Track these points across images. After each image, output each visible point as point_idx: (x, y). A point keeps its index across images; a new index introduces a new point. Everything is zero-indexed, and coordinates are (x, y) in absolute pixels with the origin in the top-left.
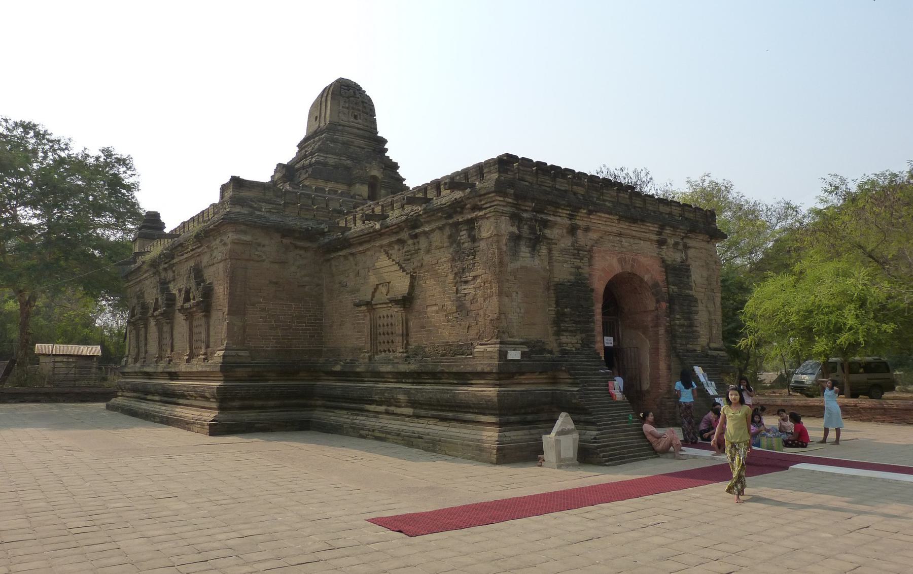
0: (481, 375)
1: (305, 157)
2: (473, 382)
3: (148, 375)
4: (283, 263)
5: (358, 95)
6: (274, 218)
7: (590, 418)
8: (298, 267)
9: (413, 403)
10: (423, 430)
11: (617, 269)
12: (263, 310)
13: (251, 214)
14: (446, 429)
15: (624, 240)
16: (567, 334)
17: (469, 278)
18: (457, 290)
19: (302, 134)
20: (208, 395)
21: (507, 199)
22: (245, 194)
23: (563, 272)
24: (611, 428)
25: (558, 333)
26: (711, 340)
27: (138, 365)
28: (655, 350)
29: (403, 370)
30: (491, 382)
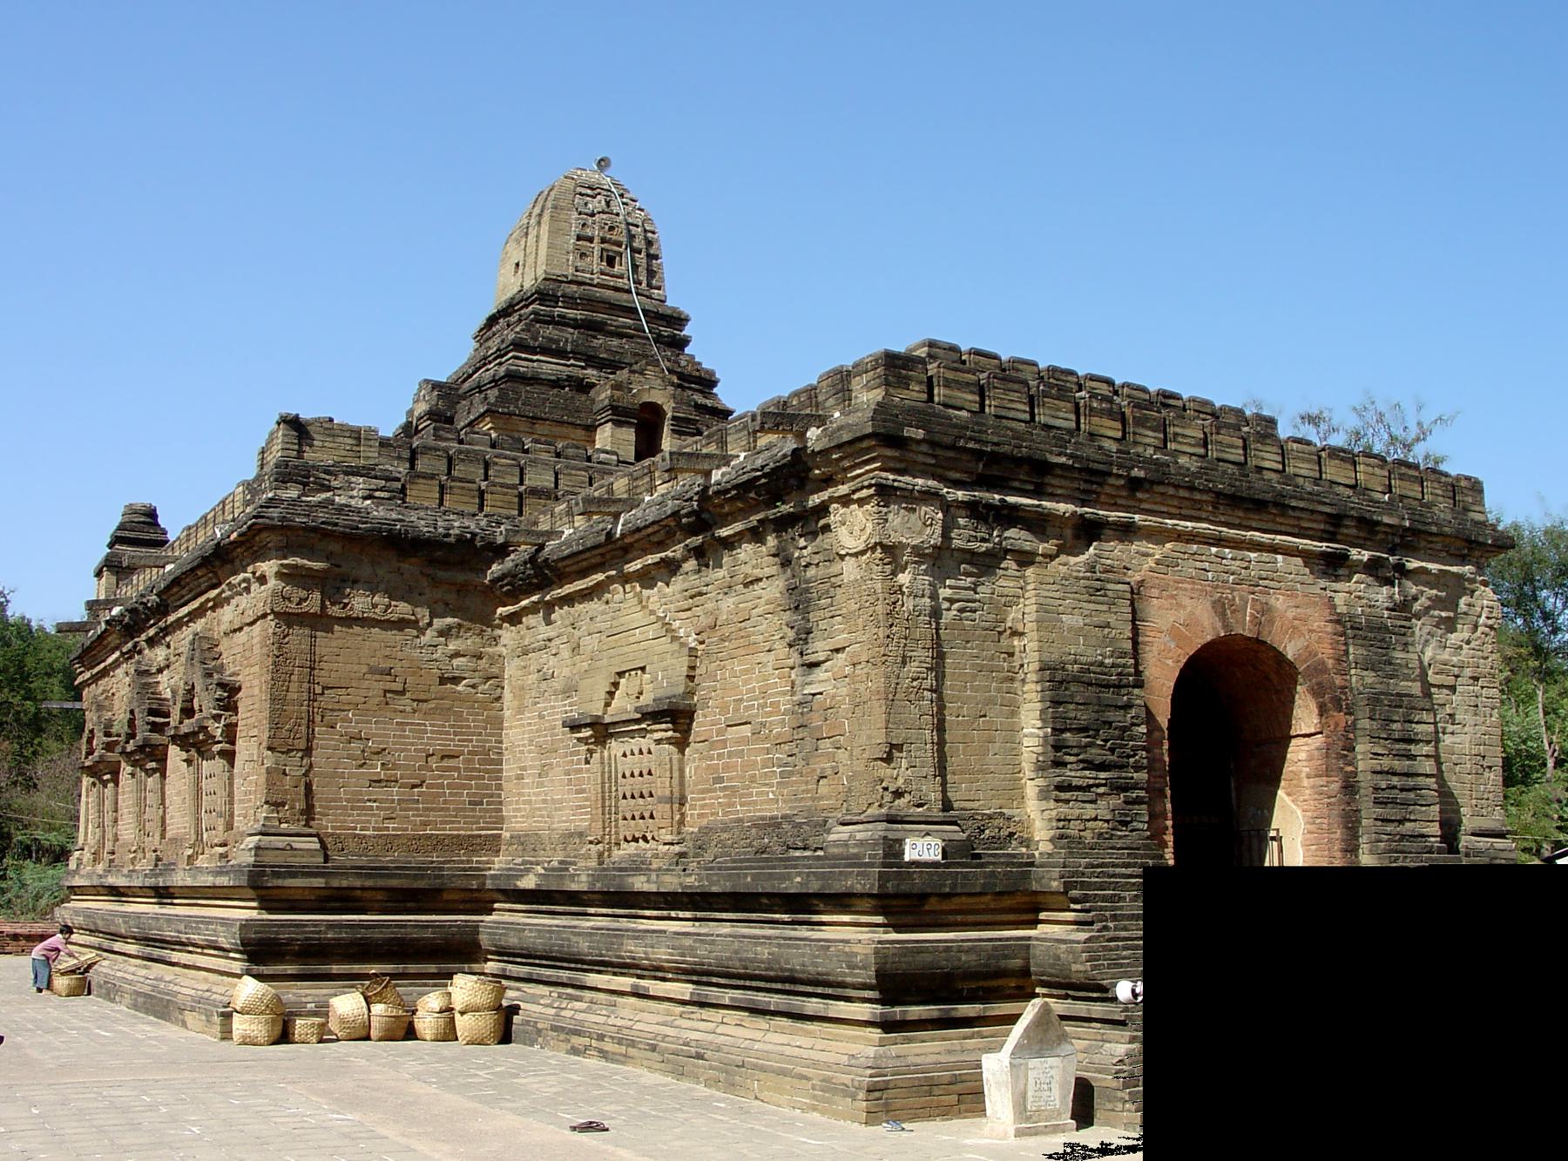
0: (841, 901)
3: (116, 892)
6: (380, 513)
8: (441, 633)
9: (697, 974)
11: (1208, 628)
14: (758, 1035)
17: (821, 656)
27: (100, 868)
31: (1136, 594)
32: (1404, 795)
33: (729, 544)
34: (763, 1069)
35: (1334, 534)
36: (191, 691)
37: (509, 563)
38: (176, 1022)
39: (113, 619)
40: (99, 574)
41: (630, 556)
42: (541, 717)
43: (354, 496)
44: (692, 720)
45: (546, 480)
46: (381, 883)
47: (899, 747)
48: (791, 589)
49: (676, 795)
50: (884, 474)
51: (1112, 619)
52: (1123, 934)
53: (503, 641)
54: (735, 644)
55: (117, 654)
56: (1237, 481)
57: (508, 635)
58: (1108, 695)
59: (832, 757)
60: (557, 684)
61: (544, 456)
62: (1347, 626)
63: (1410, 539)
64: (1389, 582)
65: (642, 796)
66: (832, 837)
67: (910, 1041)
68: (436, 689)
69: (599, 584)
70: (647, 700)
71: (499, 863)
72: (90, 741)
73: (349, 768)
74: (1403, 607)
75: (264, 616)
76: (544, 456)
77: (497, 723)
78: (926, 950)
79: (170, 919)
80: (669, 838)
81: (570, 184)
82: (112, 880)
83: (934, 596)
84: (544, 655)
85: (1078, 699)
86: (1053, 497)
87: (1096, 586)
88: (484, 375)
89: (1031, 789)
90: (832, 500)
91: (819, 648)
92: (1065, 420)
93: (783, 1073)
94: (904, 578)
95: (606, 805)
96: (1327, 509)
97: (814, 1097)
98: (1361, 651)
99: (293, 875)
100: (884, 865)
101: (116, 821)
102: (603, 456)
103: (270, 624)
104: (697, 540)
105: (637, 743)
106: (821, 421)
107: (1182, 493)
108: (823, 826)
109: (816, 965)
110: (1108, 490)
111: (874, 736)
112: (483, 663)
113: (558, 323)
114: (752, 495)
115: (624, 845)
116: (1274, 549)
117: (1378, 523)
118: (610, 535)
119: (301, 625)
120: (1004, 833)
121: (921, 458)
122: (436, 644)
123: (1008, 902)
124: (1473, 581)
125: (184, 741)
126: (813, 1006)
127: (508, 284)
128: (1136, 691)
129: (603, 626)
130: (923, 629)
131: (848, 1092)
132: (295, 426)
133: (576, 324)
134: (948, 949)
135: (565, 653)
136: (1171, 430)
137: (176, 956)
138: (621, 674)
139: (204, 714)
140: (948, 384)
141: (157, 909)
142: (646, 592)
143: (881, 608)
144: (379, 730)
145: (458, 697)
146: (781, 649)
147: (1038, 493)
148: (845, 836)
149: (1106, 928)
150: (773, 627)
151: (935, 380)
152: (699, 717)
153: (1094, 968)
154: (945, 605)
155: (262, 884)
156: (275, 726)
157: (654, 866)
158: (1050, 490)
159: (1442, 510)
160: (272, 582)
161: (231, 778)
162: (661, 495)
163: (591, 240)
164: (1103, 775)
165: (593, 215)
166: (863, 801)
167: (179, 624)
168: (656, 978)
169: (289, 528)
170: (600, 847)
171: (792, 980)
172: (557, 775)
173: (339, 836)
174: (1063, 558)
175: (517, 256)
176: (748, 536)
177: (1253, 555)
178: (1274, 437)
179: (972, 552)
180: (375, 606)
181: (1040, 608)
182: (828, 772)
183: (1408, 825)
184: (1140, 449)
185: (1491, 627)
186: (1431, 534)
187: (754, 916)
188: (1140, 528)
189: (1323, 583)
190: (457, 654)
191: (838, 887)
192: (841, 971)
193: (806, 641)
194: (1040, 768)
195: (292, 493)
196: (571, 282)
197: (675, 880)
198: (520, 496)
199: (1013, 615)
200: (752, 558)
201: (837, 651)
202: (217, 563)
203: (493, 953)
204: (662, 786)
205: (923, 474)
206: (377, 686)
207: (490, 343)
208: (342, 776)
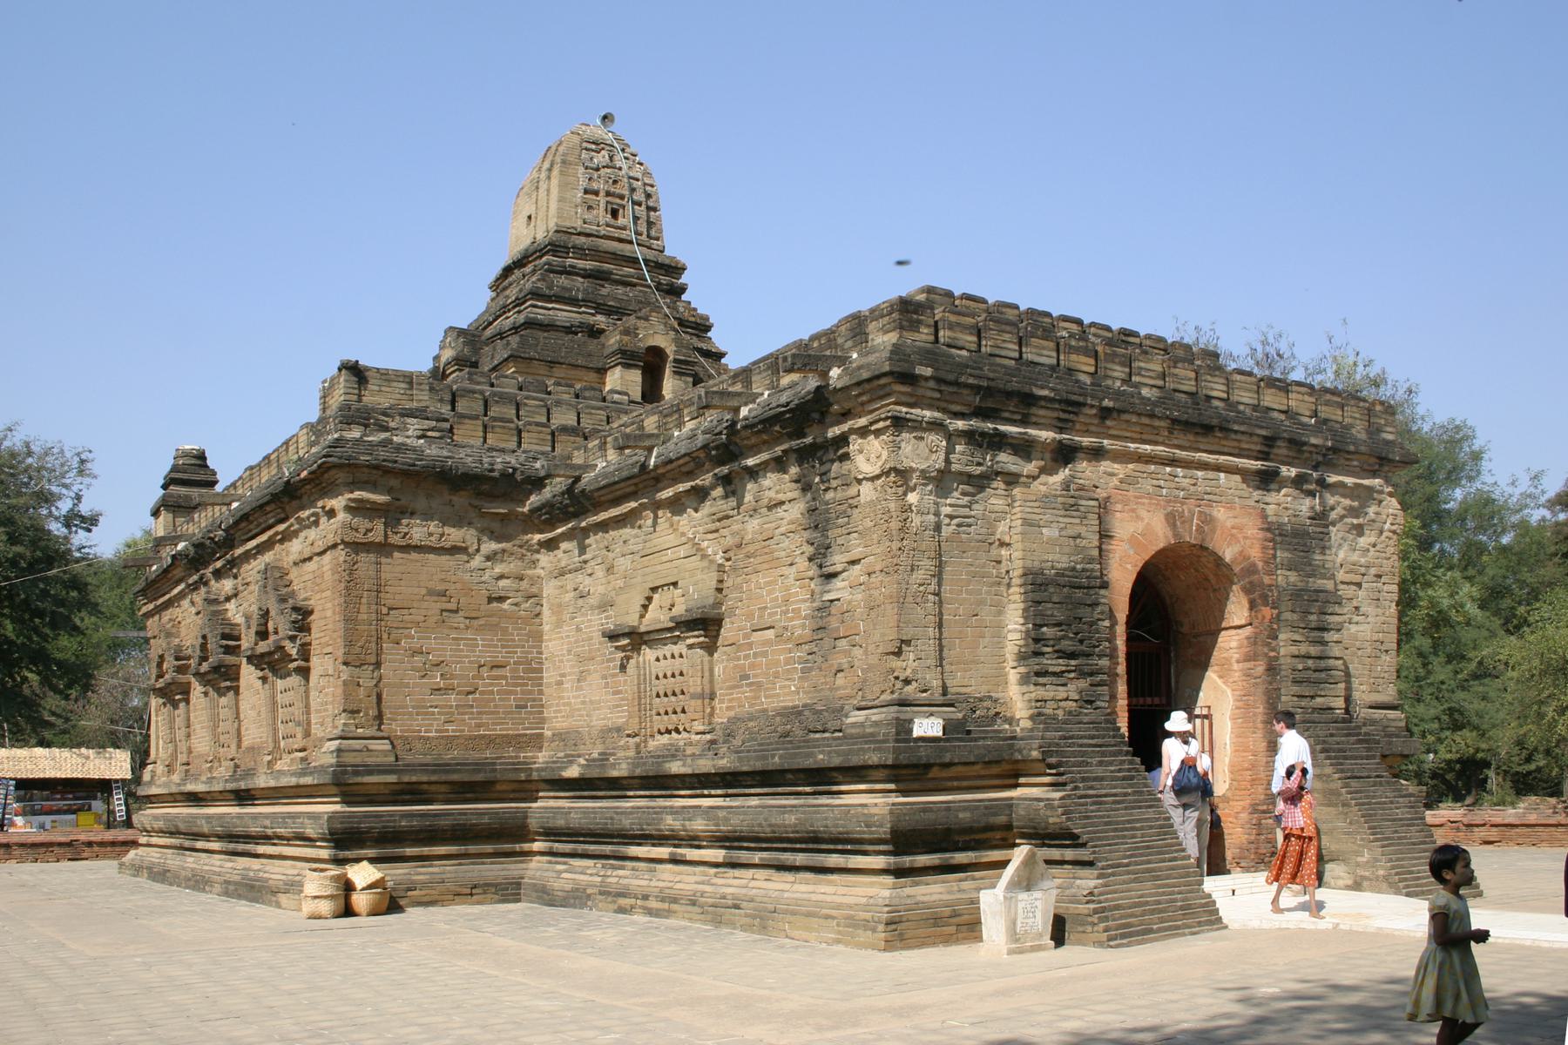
0: (857, 773)
1: (504, 309)
3: (195, 799)
6: (433, 451)
8: (488, 558)
10: (744, 891)
11: (1161, 536)
14: (787, 886)
17: (839, 568)
20: (310, 832)
24: (1128, 873)
27: (176, 778)
29: (704, 770)
31: (1104, 508)
32: (1317, 675)
33: (753, 473)
34: (794, 913)
35: (1268, 454)
36: (265, 615)
37: (547, 493)
38: (269, 903)
39: (179, 553)
40: (156, 513)
41: (660, 485)
42: (578, 629)
43: (410, 434)
44: (720, 626)
45: (571, 420)
46: (444, 778)
47: (908, 642)
48: (812, 511)
49: (707, 691)
50: (898, 408)
51: (1082, 530)
52: (1091, 792)
53: (542, 564)
54: (759, 559)
55: (182, 586)
56: (1199, 408)
57: (545, 559)
58: (1079, 594)
59: (847, 653)
60: (592, 601)
61: (566, 397)
62: (1277, 534)
63: (1333, 456)
64: (1311, 494)
65: (674, 694)
66: (849, 720)
67: (917, 884)
68: (485, 607)
69: (632, 511)
70: (680, 610)
71: (542, 757)
72: (160, 665)
73: (413, 679)
74: (1320, 517)
75: (335, 546)
76: (566, 397)
77: (538, 637)
78: (931, 810)
79: (255, 817)
80: (701, 728)
81: (576, 139)
82: (190, 787)
83: (937, 514)
84: (580, 577)
85: (1055, 599)
86: (1037, 425)
87: (1071, 500)
88: (505, 323)
89: (1013, 676)
90: (852, 431)
91: (837, 560)
92: (1048, 358)
93: (809, 915)
94: (912, 498)
95: (640, 705)
96: (1264, 432)
97: (839, 933)
98: (1286, 554)
99: (370, 773)
100: (897, 741)
101: (189, 736)
102: (616, 397)
103: (341, 554)
104: (725, 470)
105: (669, 649)
106: (842, 361)
107: (1146, 420)
108: (840, 712)
109: (836, 826)
110: (1082, 419)
111: (885, 634)
112: (524, 584)
113: (569, 273)
114: (777, 428)
115: (658, 737)
116: (1218, 468)
117: (1305, 444)
118: (644, 466)
119: (368, 552)
120: (992, 712)
121: (929, 394)
122: (483, 564)
123: (995, 770)
124: (1381, 492)
125: (256, 660)
126: (834, 860)
127: (517, 237)
128: (1102, 592)
129: (635, 548)
130: (927, 542)
131: (867, 925)
132: (356, 372)
133: (587, 275)
134: (948, 809)
135: (600, 572)
136: (1135, 364)
137: (261, 849)
138: (654, 589)
139: (281, 634)
140: (951, 327)
141: (237, 810)
142: (676, 518)
143: (895, 525)
144: (438, 645)
145: (504, 615)
146: (802, 563)
147: (1024, 422)
148: (861, 719)
149: (1076, 788)
150: (796, 547)
151: (940, 325)
152: (727, 624)
153: (1068, 819)
154: (947, 521)
155: (344, 784)
156: (349, 643)
157: (688, 752)
158: (1034, 419)
159: (1359, 431)
160: (342, 516)
161: (307, 692)
162: (688, 432)
163: (596, 193)
164: (1073, 662)
165: (597, 169)
166: (877, 689)
167: (247, 556)
168: (692, 846)
169: (356, 466)
170: (637, 739)
171: (816, 840)
172: (595, 679)
173: (407, 738)
174: (1043, 478)
175: (529, 209)
176: (773, 464)
177: (1200, 474)
178: (1220, 368)
179: (970, 476)
180: (431, 535)
181: (1023, 523)
182: (845, 666)
183: (1319, 700)
184: (1109, 382)
185: (1394, 532)
186: (1349, 452)
187: (780, 790)
188: (1107, 452)
189: (1257, 494)
190: (501, 577)
191: (855, 760)
192: (858, 830)
193: (825, 555)
194: (1022, 657)
195: (355, 433)
196: (579, 234)
197: (710, 763)
198: (553, 434)
199: (1002, 528)
200: (775, 485)
201: (853, 562)
202: (286, 499)
203: (540, 834)
204: (694, 684)
205: (930, 407)
206: (435, 606)
207: (507, 292)
208: (407, 685)
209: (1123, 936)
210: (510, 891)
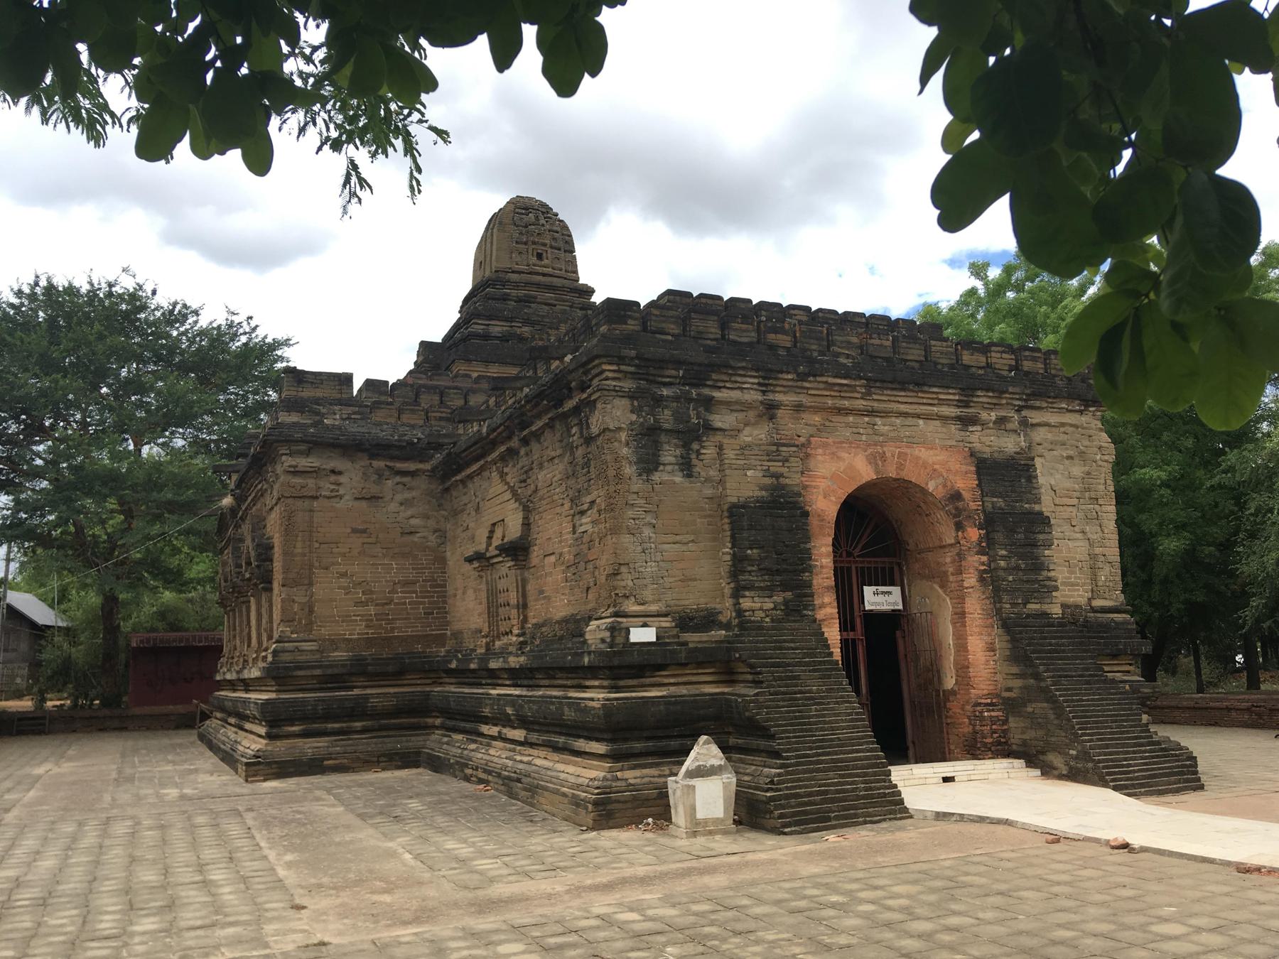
2: (588, 683)
4: (374, 499)
5: (542, 221)
6: (353, 428)
7: (775, 745)
11: (865, 473)
12: (344, 575)
13: (315, 425)
15: (879, 421)
16: (752, 593)
17: (585, 507)
18: (574, 527)
19: (466, 286)
21: (623, 368)
22: (307, 393)
23: (746, 484)
25: (737, 594)
26: (1095, 594)
28: (960, 616)
30: (606, 683)
33: (537, 436)
99: (300, 668)
164: (778, 578)
177: (898, 421)
209: (797, 823)
210: (408, 760)
